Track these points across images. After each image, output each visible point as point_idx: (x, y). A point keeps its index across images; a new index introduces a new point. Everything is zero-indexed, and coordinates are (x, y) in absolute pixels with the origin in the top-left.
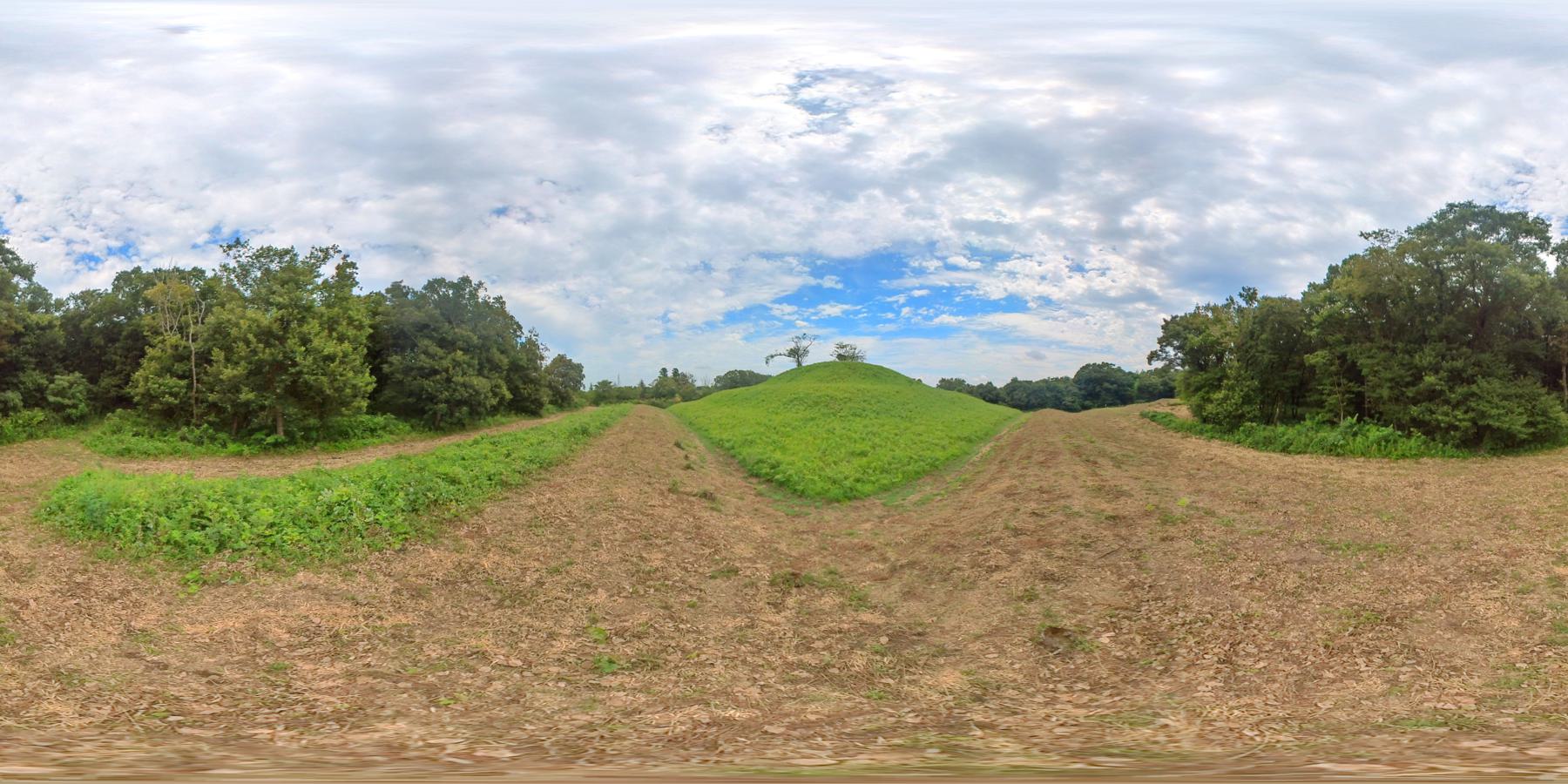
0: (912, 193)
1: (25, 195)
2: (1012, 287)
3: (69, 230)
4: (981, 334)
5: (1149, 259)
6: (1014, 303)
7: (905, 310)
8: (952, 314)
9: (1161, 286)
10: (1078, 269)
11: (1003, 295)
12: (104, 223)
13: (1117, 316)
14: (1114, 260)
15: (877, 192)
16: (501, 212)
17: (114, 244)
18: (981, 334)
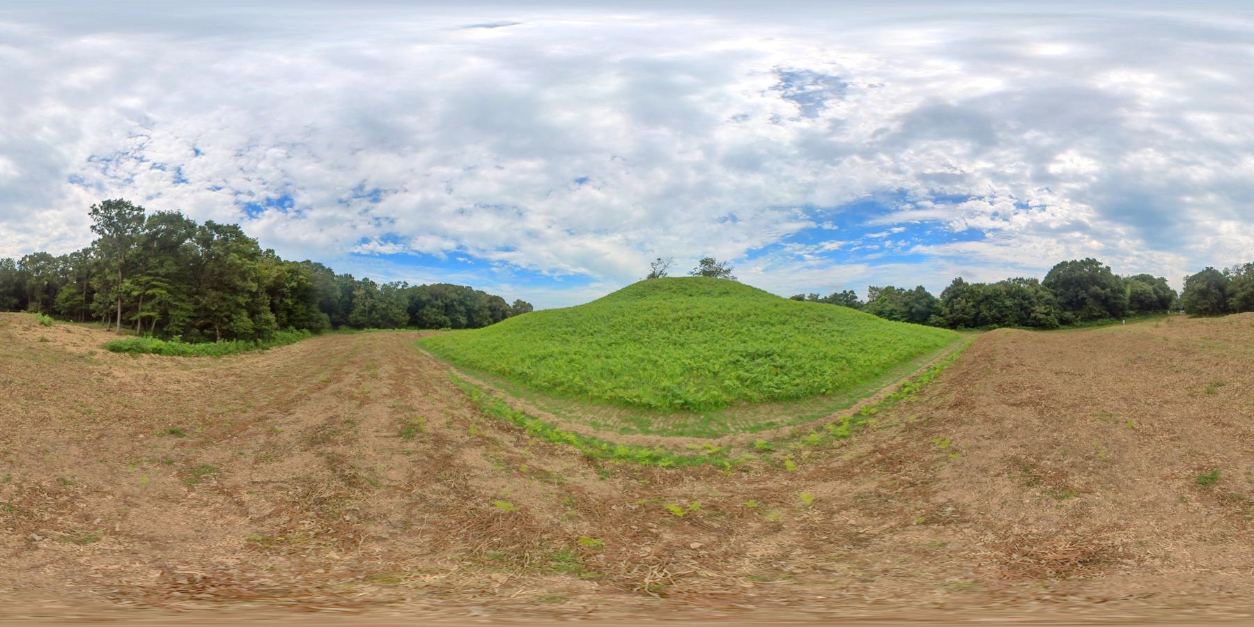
0: (884, 158)
1: (202, 150)
2: (973, 223)
3: (237, 182)
4: (948, 258)
5: (1077, 197)
6: (974, 234)
7: (888, 243)
8: (924, 244)
9: (1089, 218)
10: (1023, 206)
11: (964, 228)
12: (268, 178)
13: (1058, 242)
14: (1049, 199)
15: (856, 158)
16: (582, 181)
17: (272, 195)
18: (948, 258)
